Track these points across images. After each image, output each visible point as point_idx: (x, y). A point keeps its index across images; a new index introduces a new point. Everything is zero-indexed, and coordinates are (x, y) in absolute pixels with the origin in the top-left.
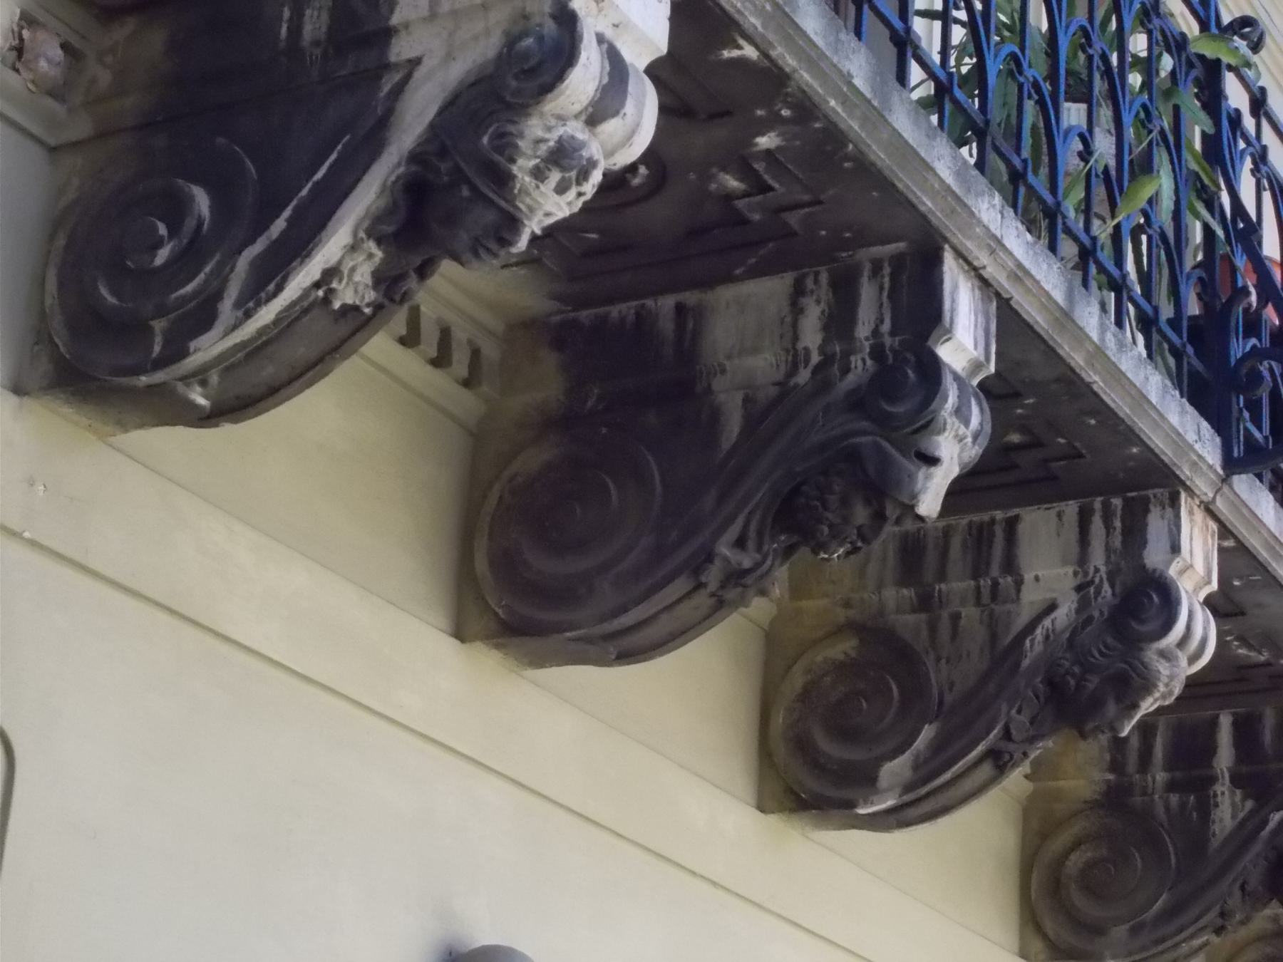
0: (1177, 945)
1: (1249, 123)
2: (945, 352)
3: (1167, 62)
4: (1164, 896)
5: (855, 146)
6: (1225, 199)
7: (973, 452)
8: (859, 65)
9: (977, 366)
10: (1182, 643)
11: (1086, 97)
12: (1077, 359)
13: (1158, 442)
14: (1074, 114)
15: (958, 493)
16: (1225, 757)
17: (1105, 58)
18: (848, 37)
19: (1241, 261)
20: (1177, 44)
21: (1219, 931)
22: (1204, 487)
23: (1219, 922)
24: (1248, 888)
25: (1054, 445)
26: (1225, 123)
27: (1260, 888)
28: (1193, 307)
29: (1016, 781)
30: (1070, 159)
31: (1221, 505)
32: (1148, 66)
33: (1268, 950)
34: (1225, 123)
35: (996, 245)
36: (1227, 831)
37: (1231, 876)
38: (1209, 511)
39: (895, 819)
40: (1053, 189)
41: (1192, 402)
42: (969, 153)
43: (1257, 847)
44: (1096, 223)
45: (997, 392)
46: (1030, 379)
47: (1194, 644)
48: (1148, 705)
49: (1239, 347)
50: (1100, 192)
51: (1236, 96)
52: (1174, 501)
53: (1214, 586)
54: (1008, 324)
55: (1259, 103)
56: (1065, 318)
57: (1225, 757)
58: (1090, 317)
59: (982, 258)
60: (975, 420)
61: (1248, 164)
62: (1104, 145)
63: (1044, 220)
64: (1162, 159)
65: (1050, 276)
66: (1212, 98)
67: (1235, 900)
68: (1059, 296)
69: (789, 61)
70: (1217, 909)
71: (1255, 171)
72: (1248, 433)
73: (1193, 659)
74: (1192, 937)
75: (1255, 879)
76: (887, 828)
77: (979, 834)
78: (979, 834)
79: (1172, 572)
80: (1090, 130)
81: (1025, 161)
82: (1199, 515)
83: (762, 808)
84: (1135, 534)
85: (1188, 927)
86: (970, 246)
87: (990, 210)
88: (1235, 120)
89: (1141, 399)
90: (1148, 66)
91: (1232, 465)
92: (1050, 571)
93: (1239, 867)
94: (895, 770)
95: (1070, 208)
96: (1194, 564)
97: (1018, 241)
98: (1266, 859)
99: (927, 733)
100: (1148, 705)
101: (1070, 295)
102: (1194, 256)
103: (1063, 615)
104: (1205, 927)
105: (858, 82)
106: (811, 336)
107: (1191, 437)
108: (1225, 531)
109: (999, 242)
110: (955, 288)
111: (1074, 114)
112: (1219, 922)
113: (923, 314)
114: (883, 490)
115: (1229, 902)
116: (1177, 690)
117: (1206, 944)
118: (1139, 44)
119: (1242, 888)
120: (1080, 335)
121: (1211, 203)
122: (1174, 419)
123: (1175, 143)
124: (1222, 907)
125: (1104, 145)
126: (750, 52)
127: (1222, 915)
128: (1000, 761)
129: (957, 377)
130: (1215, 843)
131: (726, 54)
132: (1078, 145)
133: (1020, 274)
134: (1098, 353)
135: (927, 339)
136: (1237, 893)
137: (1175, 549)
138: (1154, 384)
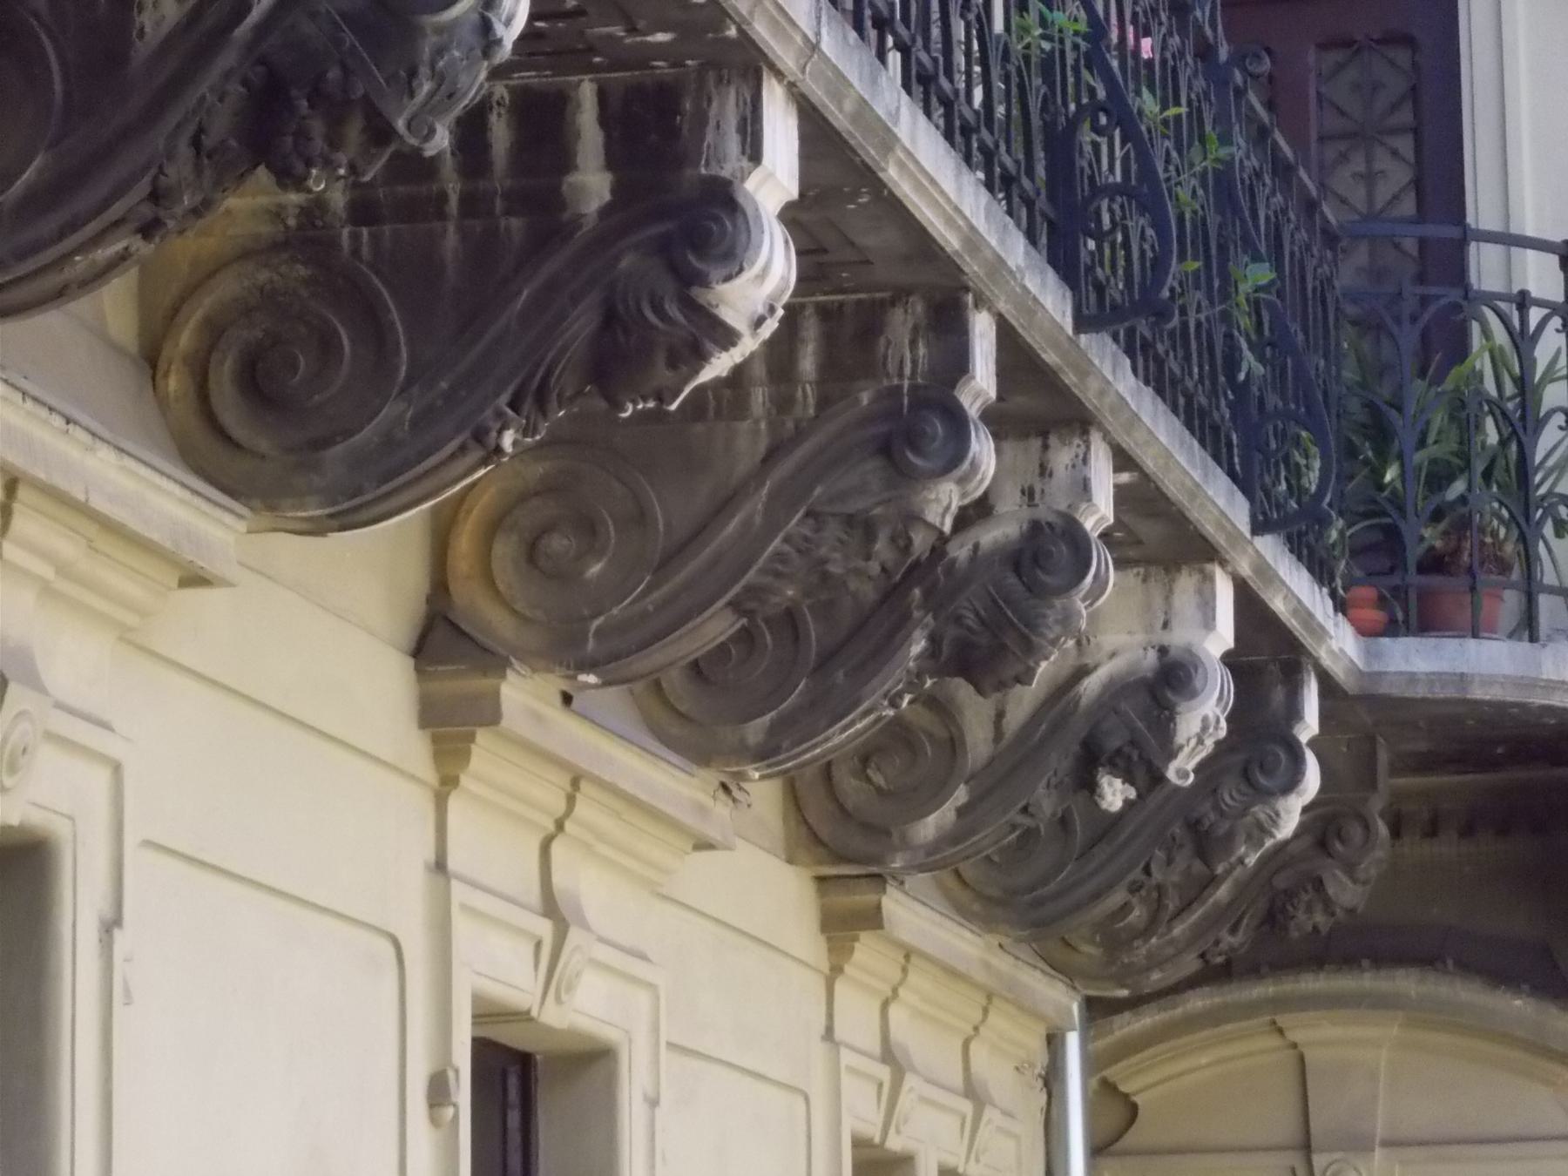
0: (67, 257)
4: (37, 162)
5: (740, 30)
21: (148, 230)
23: (147, 211)
24: (208, 142)
27: (233, 143)
33: (263, 276)
36: (165, 29)
37: (173, 118)
43: (227, 59)
67: (179, 170)
70: (143, 187)
74: (97, 240)
75: (220, 126)
81: (976, 113)
83: (790, 861)
85: (88, 221)
91: (1258, 528)
93: (190, 99)
98: (245, 82)
99: (961, 795)
104: (117, 224)
112: (147, 211)
115: (171, 170)
117: (124, 257)
119: (196, 143)
124: (155, 178)
127: (155, 196)
130: (141, 51)
135: (953, 387)
136: (184, 149)
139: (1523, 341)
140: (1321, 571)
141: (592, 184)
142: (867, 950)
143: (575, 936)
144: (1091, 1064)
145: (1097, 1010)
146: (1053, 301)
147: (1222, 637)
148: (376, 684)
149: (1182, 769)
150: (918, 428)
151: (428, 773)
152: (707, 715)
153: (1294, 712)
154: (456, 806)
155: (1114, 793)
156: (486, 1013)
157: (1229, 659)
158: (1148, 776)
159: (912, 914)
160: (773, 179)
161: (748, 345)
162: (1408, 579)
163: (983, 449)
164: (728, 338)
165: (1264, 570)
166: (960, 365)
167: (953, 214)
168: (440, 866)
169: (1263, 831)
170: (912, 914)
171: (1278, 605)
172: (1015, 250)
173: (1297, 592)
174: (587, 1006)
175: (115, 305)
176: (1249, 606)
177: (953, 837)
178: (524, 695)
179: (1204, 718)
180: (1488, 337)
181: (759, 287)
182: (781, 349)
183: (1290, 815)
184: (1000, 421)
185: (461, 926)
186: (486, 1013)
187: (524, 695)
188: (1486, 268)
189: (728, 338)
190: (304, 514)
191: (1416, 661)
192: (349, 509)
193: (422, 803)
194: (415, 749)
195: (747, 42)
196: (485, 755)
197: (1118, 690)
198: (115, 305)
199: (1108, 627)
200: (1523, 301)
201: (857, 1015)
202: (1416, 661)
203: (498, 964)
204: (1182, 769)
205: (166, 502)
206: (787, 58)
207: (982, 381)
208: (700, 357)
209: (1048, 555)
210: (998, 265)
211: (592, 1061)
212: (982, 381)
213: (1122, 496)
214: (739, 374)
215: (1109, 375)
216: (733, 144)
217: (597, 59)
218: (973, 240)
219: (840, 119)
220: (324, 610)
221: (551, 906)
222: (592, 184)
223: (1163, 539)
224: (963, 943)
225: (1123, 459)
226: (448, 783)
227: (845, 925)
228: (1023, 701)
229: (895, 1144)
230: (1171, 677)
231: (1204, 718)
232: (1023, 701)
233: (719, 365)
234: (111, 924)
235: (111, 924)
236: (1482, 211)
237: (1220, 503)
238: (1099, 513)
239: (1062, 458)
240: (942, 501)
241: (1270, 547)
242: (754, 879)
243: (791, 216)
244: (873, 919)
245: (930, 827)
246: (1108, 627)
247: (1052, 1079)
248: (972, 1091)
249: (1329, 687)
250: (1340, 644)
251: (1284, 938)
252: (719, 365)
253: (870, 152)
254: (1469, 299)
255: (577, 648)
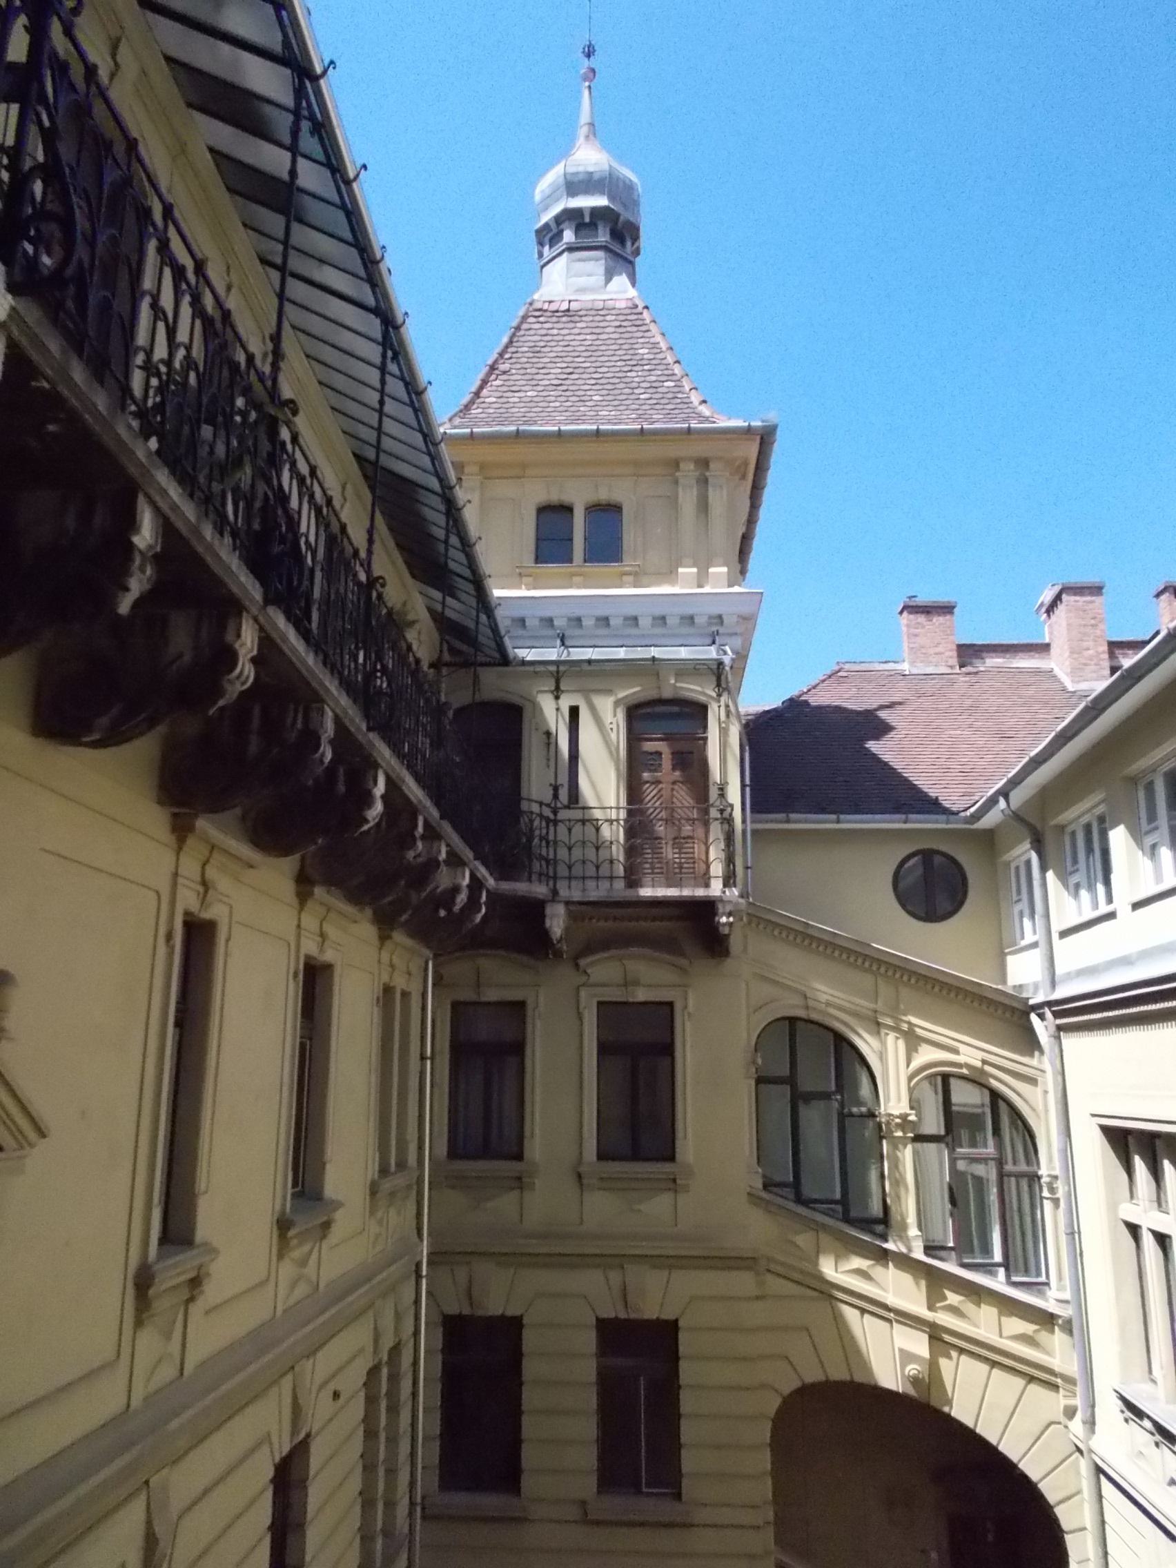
1: (289, 447)
2: (136, 540)
3: (253, 415)
6: (275, 482)
7: (147, 587)
8: (101, 401)
9: (150, 547)
10: (238, 677)
11: (211, 421)
12: (200, 549)
13: (235, 590)
14: (207, 431)
15: (136, 604)
16: (256, 722)
17: (224, 410)
18: (96, 385)
19: (280, 512)
20: (258, 407)
22: (254, 611)
25: (184, 579)
26: (278, 447)
28: (256, 526)
29: (161, 729)
30: (203, 451)
31: (261, 618)
32: (244, 414)
34: (278, 447)
35: (164, 492)
38: (256, 620)
39: (95, 745)
40: (194, 469)
41: (252, 572)
42: (153, 443)
44: (214, 484)
45: (158, 559)
46: (176, 551)
47: (243, 678)
48: (221, 703)
49: (277, 549)
50: (216, 472)
51: (285, 434)
52: (240, 615)
53: (255, 652)
54: (167, 528)
55: (295, 439)
56: (196, 531)
57: (256, 722)
58: (208, 531)
59: (157, 498)
60: (149, 572)
61: (287, 466)
62: (220, 450)
63: (186, 480)
64: (247, 459)
65: (189, 510)
66: (273, 434)
68: (192, 519)
69: (66, 393)
71: (290, 470)
72: (276, 588)
73: (243, 684)
76: (106, 746)
77: (143, 751)
78: (143, 751)
79: (237, 646)
80: (214, 441)
82: (251, 621)
84: (222, 627)
86: (152, 492)
87: (162, 477)
88: (283, 444)
89: (228, 568)
90: (244, 414)
91: (267, 601)
92: (181, 640)
94: (104, 721)
95: (202, 480)
96: (247, 642)
97: (174, 492)
100: (221, 703)
101: (198, 519)
102: (258, 504)
103: (187, 658)
105: (100, 408)
106: (70, 522)
107: (250, 588)
108: (261, 629)
109: (165, 491)
110: (143, 512)
111: (207, 431)
113: (130, 523)
114: (105, 602)
116: (235, 695)
118: (240, 402)
120: (201, 538)
121: (268, 482)
122: (243, 579)
123: (255, 454)
125: (220, 450)
126: (46, 385)
128: (152, 723)
129: (140, 551)
131: (33, 384)
132: (207, 449)
133: (175, 507)
134: (209, 547)
137: (239, 636)
138: (234, 563)
139: (531, 821)
140: (487, 867)
141: (341, 788)
142: (388, 943)
143: (210, 892)
144: (434, 967)
145: (436, 956)
146: (435, 813)
147: (467, 881)
148: (287, 887)
149: (457, 908)
150: (408, 839)
151: (175, 846)
152: (356, 897)
153: (480, 897)
154: (303, 915)
155: (442, 913)
156: (308, 957)
157: (468, 886)
158: (449, 910)
159: (399, 937)
160: (380, 788)
161: (371, 824)
162: (506, 867)
163: (420, 845)
164: (367, 821)
165: (477, 868)
166: (416, 826)
167: (416, 796)
168: (299, 926)
169: (322, 762)
170: (399, 937)
171: (479, 875)
172: (428, 803)
173: (483, 871)
174: (329, 956)
175: (238, 811)
176: (473, 876)
177: (407, 921)
178: (318, 891)
179: (462, 898)
180: (524, 820)
181: (245, 671)
182: (378, 825)
183: (478, 918)
184: (423, 837)
185: (303, 939)
186: (187, 913)
187: (318, 891)
188: (524, 806)
189: (367, 821)
190: (92, 738)
191: (506, 886)
192: (285, 851)
193: (296, 913)
194: (294, 901)
195: (376, 761)
196: (310, 904)
197: (445, 891)
198: (238, 811)
199: (444, 879)
200: (532, 813)
201: (385, 956)
202: (506, 886)
203: (310, 947)
204: (457, 908)
205: (245, 850)
206: (383, 764)
207: (420, 829)
208: (361, 826)
209: (432, 865)
210: (425, 807)
211: (328, 968)
212: (420, 829)
213: (448, 853)
214: (370, 829)
215: (447, 828)
216: (371, 783)
217: (51, 428)
218: (420, 801)
219: (394, 776)
220: (277, 874)
221: (204, 883)
222: (341, 788)
223: (455, 861)
224: (409, 942)
225: (448, 845)
226: (380, 949)
227: (384, 938)
228: (424, 894)
229: (206, 915)
230: (456, 890)
231: (462, 898)
232: (424, 894)
233: (366, 827)
234: (228, 940)
235: (228, 940)
236: (524, 793)
237: (468, 854)
238: (443, 856)
239: (435, 845)
240: (410, 855)
241: (477, 863)
242: (366, 930)
243: (383, 797)
244: (389, 937)
245: (404, 917)
246: (444, 879)
247: (426, 969)
248: (409, 974)
249: (488, 891)
250: (491, 882)
251: (478, 942)
252: (366, 827)
253: (400, 783)
254: (521, 813)
255: (331, 881)
